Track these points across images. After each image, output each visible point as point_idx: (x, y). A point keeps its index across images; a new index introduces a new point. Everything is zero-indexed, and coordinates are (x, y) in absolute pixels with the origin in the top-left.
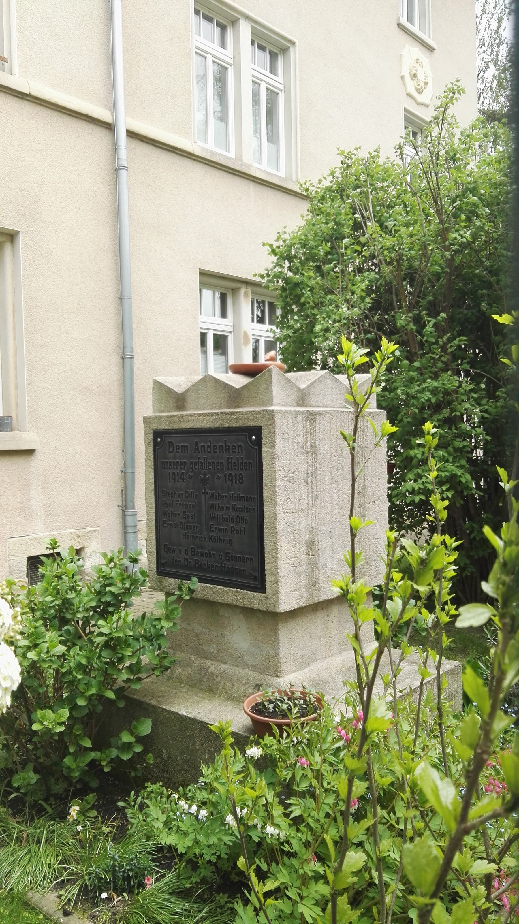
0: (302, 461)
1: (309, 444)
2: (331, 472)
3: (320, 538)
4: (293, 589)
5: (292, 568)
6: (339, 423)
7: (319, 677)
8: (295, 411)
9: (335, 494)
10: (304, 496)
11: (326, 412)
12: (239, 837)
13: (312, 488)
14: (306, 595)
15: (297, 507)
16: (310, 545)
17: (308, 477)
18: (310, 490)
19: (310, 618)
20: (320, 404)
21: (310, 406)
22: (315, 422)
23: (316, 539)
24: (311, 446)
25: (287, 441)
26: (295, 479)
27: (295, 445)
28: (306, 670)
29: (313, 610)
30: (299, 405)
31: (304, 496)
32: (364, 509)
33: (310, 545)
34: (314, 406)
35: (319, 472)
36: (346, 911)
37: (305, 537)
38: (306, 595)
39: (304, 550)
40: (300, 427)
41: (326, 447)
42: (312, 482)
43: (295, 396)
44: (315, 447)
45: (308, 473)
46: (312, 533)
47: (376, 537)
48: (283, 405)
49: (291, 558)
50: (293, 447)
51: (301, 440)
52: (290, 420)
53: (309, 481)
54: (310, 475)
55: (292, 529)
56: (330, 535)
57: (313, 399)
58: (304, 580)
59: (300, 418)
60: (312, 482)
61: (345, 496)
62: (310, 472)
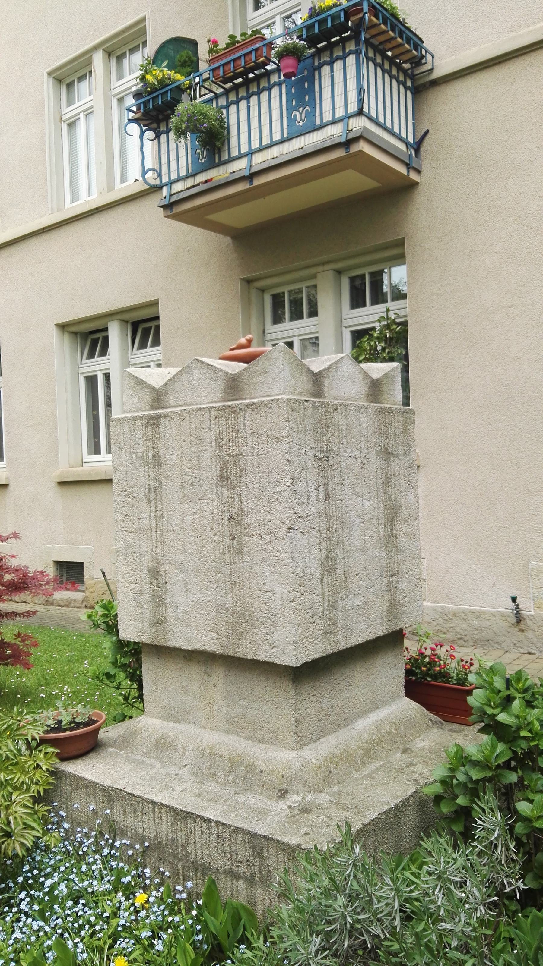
0: (142, 474)
1: (150, 454)
2: (183, 487)
3: (167, 568)
4: (133, 618)
5: (131, 594)
6: (193, 425)
7: (174, 739)
8: (133, 417)
9: (188, 517)
10: (145, 515)
11: (174, 413)
12: (29, 811)
13: (156, 507)
14: (149, 631)
15: (137, 527)
16: (155, 574)
17: (150, 492)
18: (153, 509)
19: (180, 665)
20: (181, 403)
21: (167, 408)
22: (158, 426)
23: (162, 569)
24: (154, 456)
25: (123, 451)
26: (134, 495)
27: (134, 456)
28: (171, 724)
29: (185, 657)
30: (153, 408)
31: (145, 515)
32: (239, 544)
33: (155, 574)
34: (173, 407)
35: (164, 487)
36: (21, 921)
37: (147, 563)
38: (149, 631)
39: (146, 578)
40: (139, 434)
41: (174, 457)
42: (155, 499)
43: (148, 397)
44: (160, 457)
45: (150, 489)
46: (155, 559)
47: (266, 588)
48: (134, 411)
49: (131, 583)
50: (131, 458)
51: (140, 450)
52: (126, 428)
53: (152, 497)
54: (153, 490)
55: (132, 551)
56: (182, 567)
57: (171, 399)
58: (147, 613)
59: (139, 423)
60: (155, 499)
61: (204, 521)
62: (152, 487)
